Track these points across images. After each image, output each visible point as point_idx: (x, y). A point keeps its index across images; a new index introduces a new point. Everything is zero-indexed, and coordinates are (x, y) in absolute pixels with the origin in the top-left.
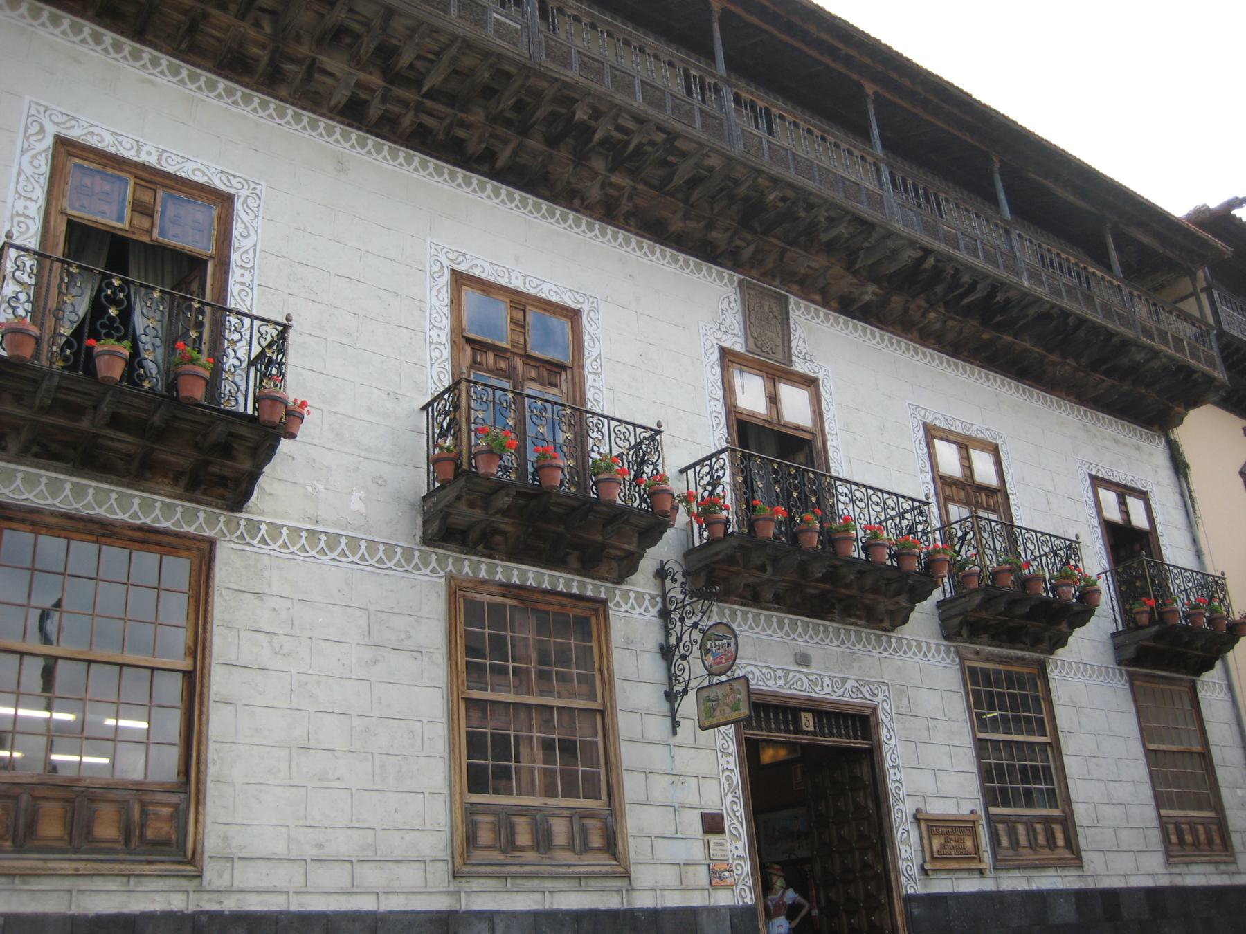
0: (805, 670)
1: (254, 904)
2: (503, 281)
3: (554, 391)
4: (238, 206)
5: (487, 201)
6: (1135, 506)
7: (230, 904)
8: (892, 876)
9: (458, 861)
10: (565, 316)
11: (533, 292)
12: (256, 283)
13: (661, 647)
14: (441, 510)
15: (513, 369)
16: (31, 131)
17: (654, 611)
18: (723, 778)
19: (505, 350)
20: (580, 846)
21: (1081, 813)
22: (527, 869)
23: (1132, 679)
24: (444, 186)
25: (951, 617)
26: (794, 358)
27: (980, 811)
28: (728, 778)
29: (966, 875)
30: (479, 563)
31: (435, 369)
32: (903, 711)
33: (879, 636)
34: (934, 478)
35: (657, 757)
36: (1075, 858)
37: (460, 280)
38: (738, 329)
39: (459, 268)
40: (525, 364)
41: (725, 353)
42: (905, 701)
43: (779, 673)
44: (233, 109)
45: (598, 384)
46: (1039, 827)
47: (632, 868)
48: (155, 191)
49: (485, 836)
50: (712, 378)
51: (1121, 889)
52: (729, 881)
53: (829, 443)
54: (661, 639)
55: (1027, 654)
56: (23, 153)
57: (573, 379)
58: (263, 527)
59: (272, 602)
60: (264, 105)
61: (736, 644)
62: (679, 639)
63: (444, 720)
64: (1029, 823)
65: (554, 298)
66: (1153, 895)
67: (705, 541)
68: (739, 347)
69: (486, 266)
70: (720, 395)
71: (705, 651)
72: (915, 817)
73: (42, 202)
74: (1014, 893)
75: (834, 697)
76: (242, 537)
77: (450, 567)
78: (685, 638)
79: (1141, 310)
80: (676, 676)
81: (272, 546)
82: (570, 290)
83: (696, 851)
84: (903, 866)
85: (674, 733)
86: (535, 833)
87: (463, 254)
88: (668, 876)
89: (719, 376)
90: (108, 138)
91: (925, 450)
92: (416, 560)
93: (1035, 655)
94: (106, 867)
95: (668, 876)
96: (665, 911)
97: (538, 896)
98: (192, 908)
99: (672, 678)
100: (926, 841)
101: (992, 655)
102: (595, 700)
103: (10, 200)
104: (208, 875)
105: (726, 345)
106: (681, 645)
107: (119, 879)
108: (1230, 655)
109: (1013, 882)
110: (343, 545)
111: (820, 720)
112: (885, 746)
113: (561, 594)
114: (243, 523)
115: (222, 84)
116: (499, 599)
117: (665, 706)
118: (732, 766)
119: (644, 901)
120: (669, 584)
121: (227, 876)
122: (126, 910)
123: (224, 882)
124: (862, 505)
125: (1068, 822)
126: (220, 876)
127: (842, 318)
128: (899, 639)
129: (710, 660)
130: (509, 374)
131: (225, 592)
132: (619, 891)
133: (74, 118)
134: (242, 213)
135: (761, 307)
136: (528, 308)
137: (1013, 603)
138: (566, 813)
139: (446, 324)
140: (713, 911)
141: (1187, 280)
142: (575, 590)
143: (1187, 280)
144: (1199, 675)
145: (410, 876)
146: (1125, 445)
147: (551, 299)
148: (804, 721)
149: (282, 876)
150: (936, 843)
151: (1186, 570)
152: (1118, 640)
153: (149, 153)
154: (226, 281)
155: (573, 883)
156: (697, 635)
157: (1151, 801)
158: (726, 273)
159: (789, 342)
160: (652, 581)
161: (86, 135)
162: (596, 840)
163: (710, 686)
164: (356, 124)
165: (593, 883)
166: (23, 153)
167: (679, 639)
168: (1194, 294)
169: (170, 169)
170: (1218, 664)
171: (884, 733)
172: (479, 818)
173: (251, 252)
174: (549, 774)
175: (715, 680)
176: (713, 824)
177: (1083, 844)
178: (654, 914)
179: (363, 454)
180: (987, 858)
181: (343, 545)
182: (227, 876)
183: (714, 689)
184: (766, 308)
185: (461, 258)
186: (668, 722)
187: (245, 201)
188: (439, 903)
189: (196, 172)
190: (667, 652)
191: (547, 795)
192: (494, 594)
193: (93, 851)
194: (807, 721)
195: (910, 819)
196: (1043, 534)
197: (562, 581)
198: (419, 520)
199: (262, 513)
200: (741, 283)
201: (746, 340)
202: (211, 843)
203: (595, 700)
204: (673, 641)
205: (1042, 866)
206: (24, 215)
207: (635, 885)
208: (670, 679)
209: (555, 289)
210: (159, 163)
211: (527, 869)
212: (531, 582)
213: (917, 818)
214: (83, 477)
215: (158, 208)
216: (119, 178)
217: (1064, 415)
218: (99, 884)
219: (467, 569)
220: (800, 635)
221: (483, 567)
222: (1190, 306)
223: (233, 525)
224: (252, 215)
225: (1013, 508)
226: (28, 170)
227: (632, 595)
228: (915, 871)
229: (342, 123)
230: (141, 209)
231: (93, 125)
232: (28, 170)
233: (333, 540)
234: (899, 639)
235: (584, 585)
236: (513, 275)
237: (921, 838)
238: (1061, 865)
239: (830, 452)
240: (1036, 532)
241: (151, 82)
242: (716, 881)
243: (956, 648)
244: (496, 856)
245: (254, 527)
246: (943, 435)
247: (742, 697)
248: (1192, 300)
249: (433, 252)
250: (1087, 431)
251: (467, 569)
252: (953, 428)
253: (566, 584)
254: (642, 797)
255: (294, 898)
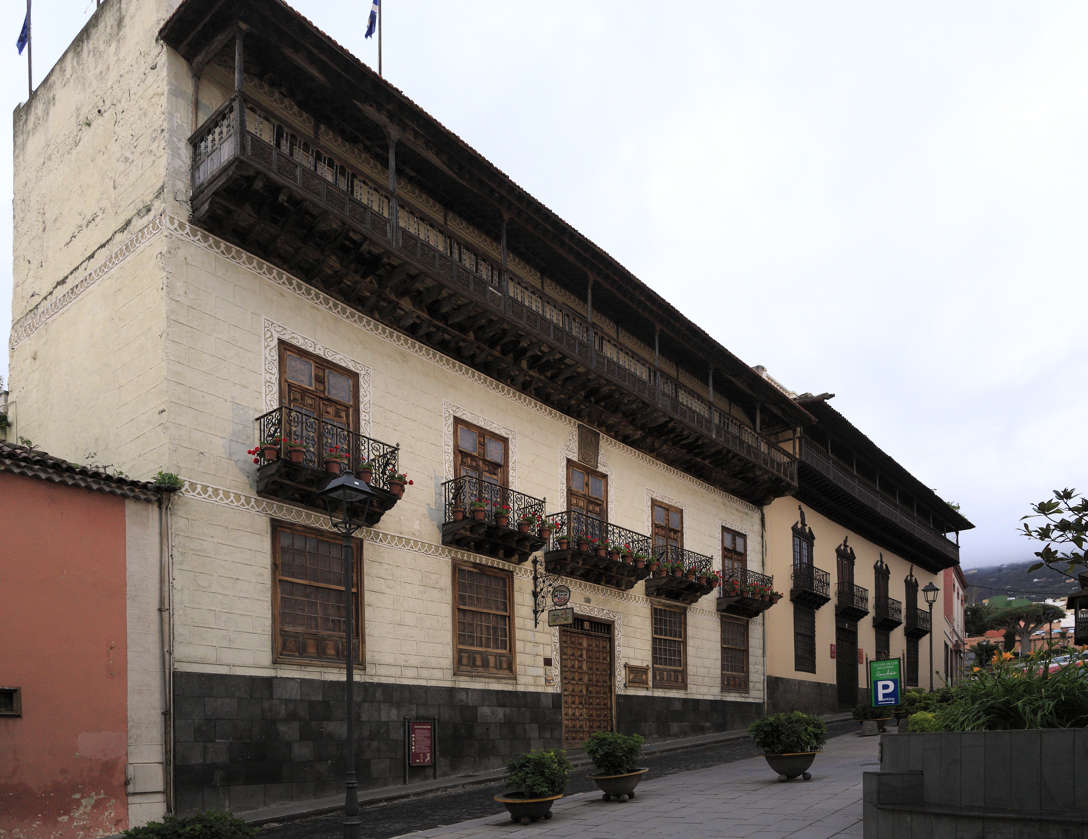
0: (588, 604)
1: (384, 680)
2: (475, 422)
3: (495, 477)
4: (361, 379)
5: (469, 379)
6: (739, 541)
7: (376, 680)
8: (613, 687)
9: (455, 669)
10: (501, 440)
11: (488, 428)
12: (371, 420)
13: (533, 592)
14: (454, 531)
15: (478, 466)
16: (267, 336)
17: (531, 577)
18: (553, 645)
19: (476, 457)
20: (499, 667)
21: (690, 670)
22: (479, 674)
23: (722, 617)
24: (450, 371)
25: (651, 587)
26: (599, 465)
27: (651, 666)
28: (555, 645)
29: (641, 689)
30: (464, 553)
31: (447, 466)
32: (625, 624)
33: (619, 593)
34: (652, 524)
35: (529, 635)
36: (685, 687)
37: (457, 421)
38: (576, 450)
39: (457, 415)
40: (483, 464)
41: (569, 460)
42: (626, 620)
43: (578, 605)
44: (354, 324)
45: (514, 475)
46: (672, 674)
47: (518, 676)
48: (324, 370)
49: (465, 661)
50: (562, 473)
51: (701, 700)
52: (552, 684)
53: (609, 506)
54: (533, 589)
55: (679, 604)
56: (265, 348)
57: (504, 472)
58: (381, 534)
59: (386, 566)
60: (368, 323)
61: (570, 595)
62: (542, 590)
63: (451, 616)
64: (669, 671)
65: (497, 432)
66: (714, 704)
67: (555, 549)
68: (575, 459)
69: (469, 414)
70: (565, 481)
71: (554, 595)
72: (624, 666)
73: (277, 375)
74: (659, 697)
75: (598, 616)
76: (372, 538)
77: (453, 555)
78: (545, 589)
79: (764, 448)
80: (539, 604)
81: (384, 543)
82: (504, 428)
83: (541, 672)
84: (617, 684)
85: (536, 627)
86: (483, 661)
87: (458, 408)
88: (531, 680)
89: (565, 472)
90: (301, 340)
91: (650, 511)
92: (440, 551)
93: (683, 605)
94: (332, 665)
95: (531, 680)
96: (528, 692)
97: (484, 684)
98: (363, 681)
99: (536, 604)
100: (627, 675)
101: (665, 603)
102: (506, 611)
103: (263, 374)
104: (367, 669)
105: (569, 457)
106: (542, 592)
107: (337, 669)
108: (767, 612)
109: (659, 693)
110: (412, 544)
111: (591, 625)
112: (616, 638)
113: (495, 568)
114: (372, 532)
115: (349, 310)
116: (472, 569)
117: (533, 616)
118: (556, 641)
119: (521, 688)
120: (538, 566)
121: (374, 670)
122: (340, 680)
123: (373, 672)
124: (623, 538)
125: (684, 673)
126: (372, 670)
127: (622, 445)
128: (627, 594)
129: (556, 600)
130: (476, 468)
131: (367, 561)
132: (512, 684)
133: (285, 329)
134: (362, 383)
135: (587, 439)
136: (486, 436)
137: (681, 582)
138: (494, 654)
139: (451, 443)
140: (546, 694)
141: (791, 431)
142: (501, 567)
143: (791, 431)
144: (751, 617)
145: (438, 674)
146: (741, 512)
147: (496, 432)
148: (585, 625)
149: (394, 671)
150: (631, 676)
151: (757, 573)
152: (719, 601)
153: (320, 349)
154: (359, 419)
155: (496, 680)
156: (551, 589)
157: (720, 667)
158: (573, 420)
159: (598, 456)
160: (531, 564)
161: (291, 338)
162: (505, 666)
163: (555, 610)
164: (411, 335)
165: (503, 681)
166: (265, 348)
167: (542, 590)
168: (793, 439)
169: (330, 359)
170: (761, 614)
171: (616, 632)
172: (463, 654)
173: (368, 404)
174: (488, 639)
175: (557, 607)
176: (548, 662)
177: (689, 681)
178: (524, 693)
179: (418, 504)
180: (650, 683)
181: (412, 544)
182: (374, 670)
183: (557, 611)
184: (589, 439)
185: (458, 410)
186: (534, 622)
187: (364, 377)
188: (448, 684)
189: (342, 361)
190: (535, 594)
191: (486, 647)
192: (470, 567)
193: (327, 658)
194: (587, 625)
195: (622, 666)
196: (698, 554)
197: (496, 562)
198: (441, 535)
199: (379, 528)
200: (579, 425)
201: (579, 455)
202: (368, 658)
203: (506, 611)
204: (538, 590)
205: (671, 688)
206: (270, 382)
207: (518, 683)
208: (536, 605)
209: (498, 427)
210: (324, 355)
211: (479, 674)
212: (484, 562)
213: (626, 666)
214: (309, 510)
215: (326, 379)
216: (308, 363)
217: (715, 496)
218: (330, 670)
219: (459, 556)
220: (587, 590)
221: (466, 555)
222: (784, 446)
223: (369, 533)
224: (367, 385)
225: (684, 540)
226: (269, 358)
227: (523, 570)
228: (622, 686)
229: (404, 334)
230: (320, 380)
231: (293, 333)
232: (269, 358)
233: (408, 541)
234: (627, 594)
235: (504, 565)
236: (480, 419)
237: (626, 674)
238: (679, 688)
239: (609, 510)
240: (695, 553)
241: (316, 308)
242: (547, 683)
243: (651, 599)
244: (469, 669)
245: (377, 534)
246: (659, 504)
247: (570, 616)
248: (791, 442)
249: (446, 406)
250: (724, 505)
251: (459, 556)
252: (664, 501)
253: (497, 564)
254: (522, 651)
255: (398, 679)
